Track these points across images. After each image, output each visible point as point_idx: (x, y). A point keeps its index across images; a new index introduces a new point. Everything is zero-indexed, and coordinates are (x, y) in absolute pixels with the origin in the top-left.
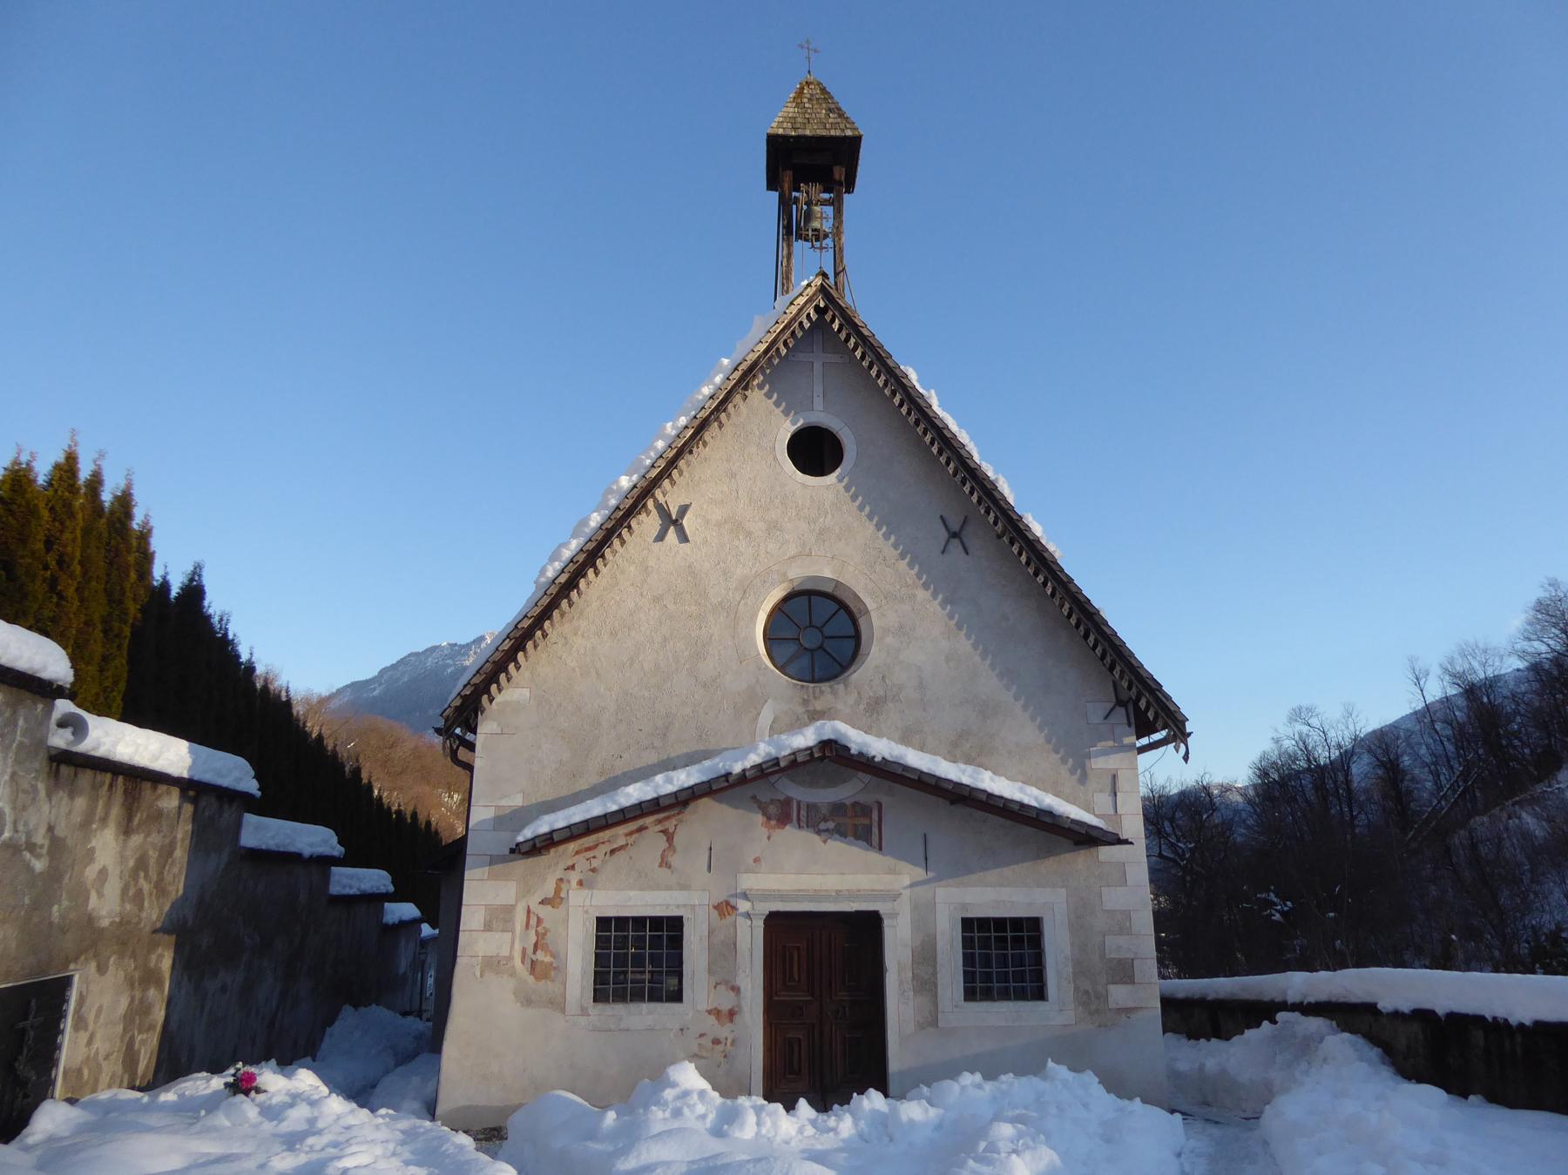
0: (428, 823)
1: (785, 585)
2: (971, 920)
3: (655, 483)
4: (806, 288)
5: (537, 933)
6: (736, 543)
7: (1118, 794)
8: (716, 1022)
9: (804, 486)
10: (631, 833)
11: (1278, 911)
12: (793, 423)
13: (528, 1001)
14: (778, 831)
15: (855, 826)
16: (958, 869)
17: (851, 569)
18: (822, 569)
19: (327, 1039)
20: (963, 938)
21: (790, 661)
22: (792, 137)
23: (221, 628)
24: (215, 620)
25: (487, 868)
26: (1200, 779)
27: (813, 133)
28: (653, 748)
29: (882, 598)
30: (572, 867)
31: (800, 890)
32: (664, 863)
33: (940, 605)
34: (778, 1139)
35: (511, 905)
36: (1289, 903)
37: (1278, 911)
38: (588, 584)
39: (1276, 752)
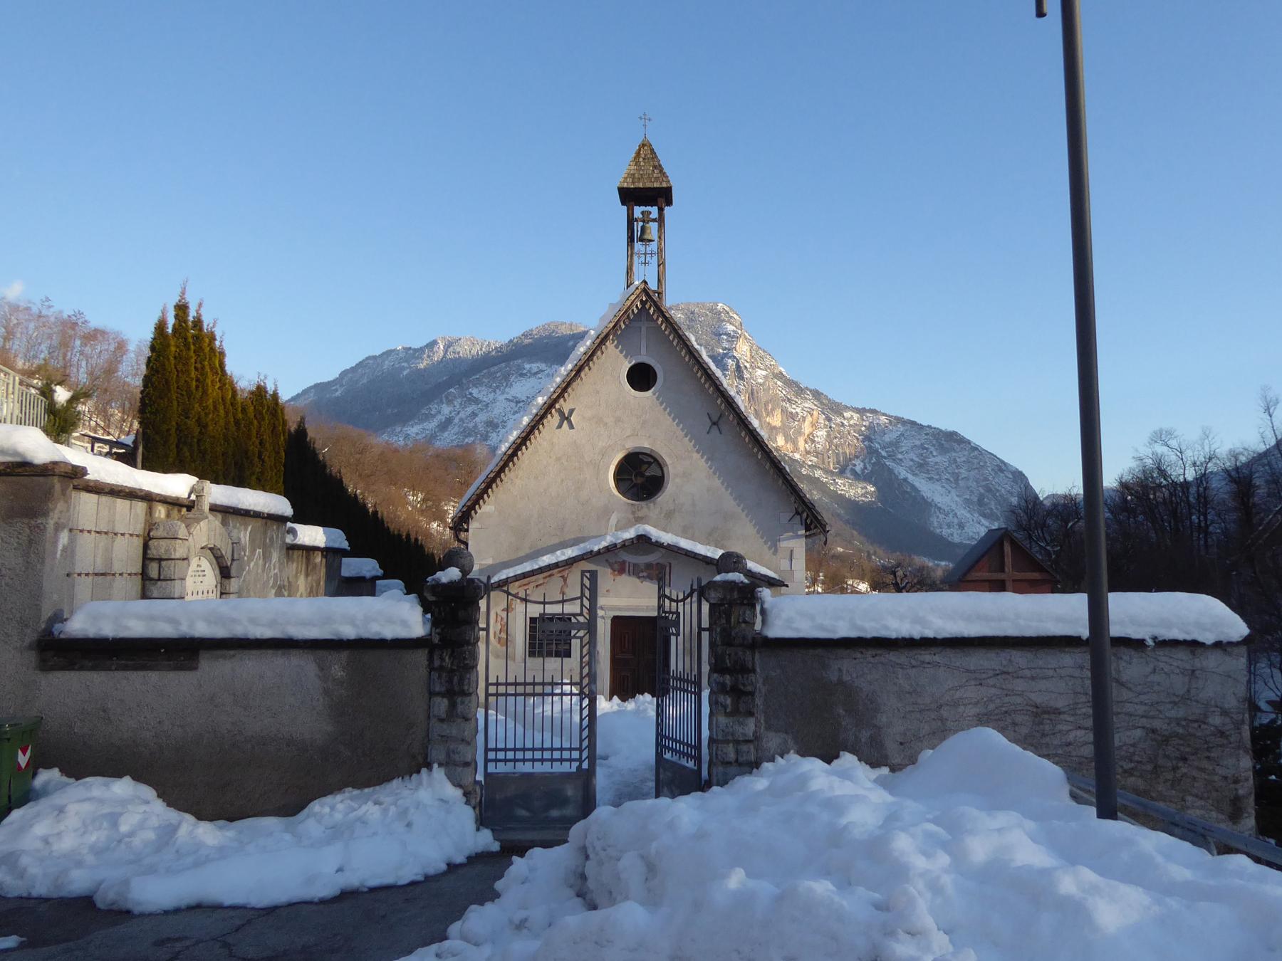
0: (416, 540)
3: (556, 400)
5: (501, 624)
7: (793, 560)
18: (644, 444)
38: (523, 454)
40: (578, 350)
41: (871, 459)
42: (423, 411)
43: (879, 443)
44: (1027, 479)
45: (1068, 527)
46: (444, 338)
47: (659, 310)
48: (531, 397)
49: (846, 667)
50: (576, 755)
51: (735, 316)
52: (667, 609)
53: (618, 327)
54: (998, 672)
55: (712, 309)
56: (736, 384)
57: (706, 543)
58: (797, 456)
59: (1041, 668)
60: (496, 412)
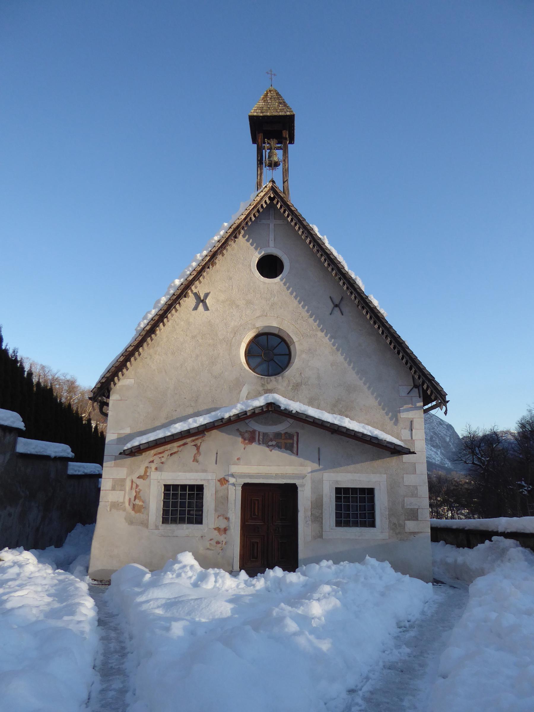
1: (255, 330)
2: (340, 489)
4: (264, 188)
5: (136, 491)
7: (413, 430)
8: (218, 534)
9: (265, 283)
10: (179, 446)
11: (525, 490)
12: (259, 253)
13: (131, 522)
14: (249, 445)
15: (286, 444)
16: (334, 465)
17: (286, 322)
19: (68, 538)
20: (336, 497)
21: (259, 365)
22: (261, 116)
23: (14, 355)
24: (10, 352)
25: (114, 461)
26: (492, 428)
27: (271, 114)
28: (191, 407)
29: (301, 336)
30: (153, 462)
31: (259, 473)
32: (195, 460)
33: (328, 339)
34: (223, 589)
35: (124, 479)
36: (531, 486)
37: (525, 490)
39: (529, 416)
44: (454, 428)
45: (494, 447)
47: (286, 206)
53: (248, 219)
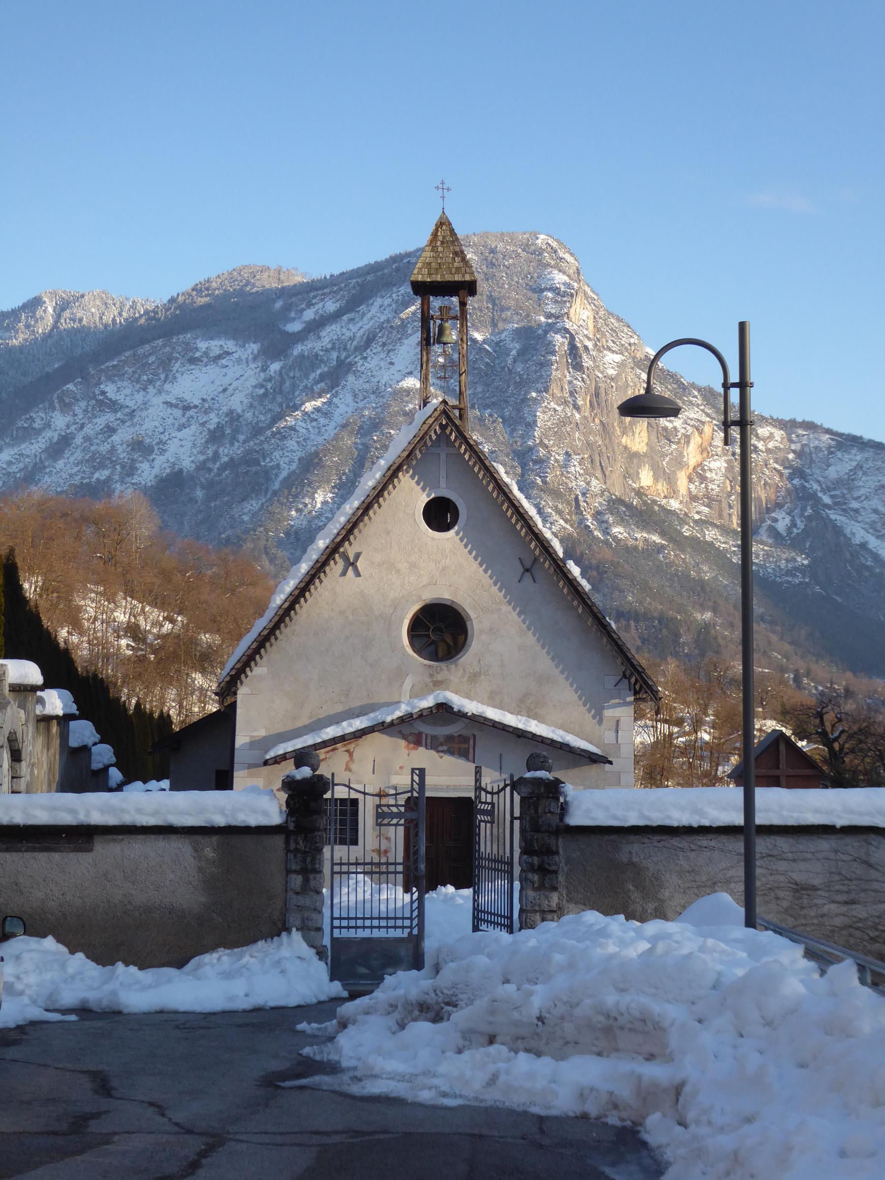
3: (340, 544)
6: (390, 577)
9: (433, 539)
10: (327, 752)
12: (428, 496)
38: (301, 607)
40: (366, 484)
41: (804, 509)
42: (20, 424)
43: (818, 482)
46: (54, 294)
48: (209, 399)
49: (634, 850)
50: (407, 923)
51: (567, 256)
52: (483, 800)
53: (412, 456)
54: (764, 855)
55: (527, 245)
56: (568, 378)
57: (517, 712)
58: (674, 505)
59: (801, 852)
60: (148, 425)
